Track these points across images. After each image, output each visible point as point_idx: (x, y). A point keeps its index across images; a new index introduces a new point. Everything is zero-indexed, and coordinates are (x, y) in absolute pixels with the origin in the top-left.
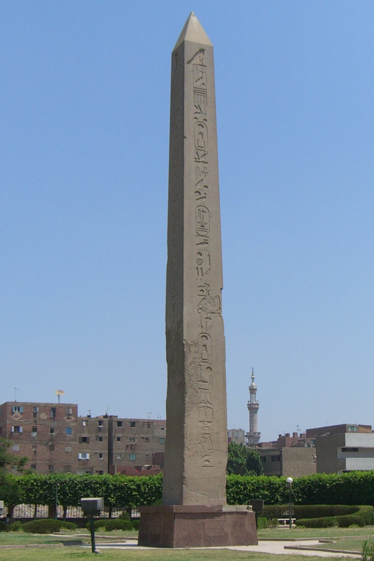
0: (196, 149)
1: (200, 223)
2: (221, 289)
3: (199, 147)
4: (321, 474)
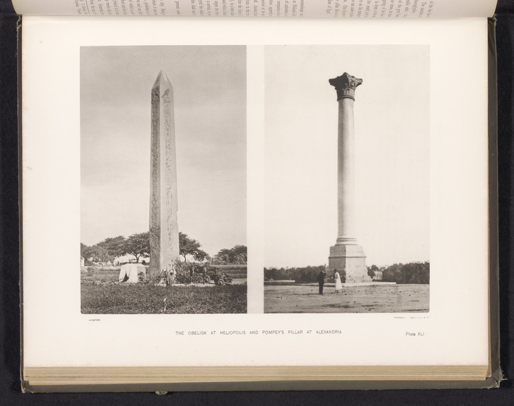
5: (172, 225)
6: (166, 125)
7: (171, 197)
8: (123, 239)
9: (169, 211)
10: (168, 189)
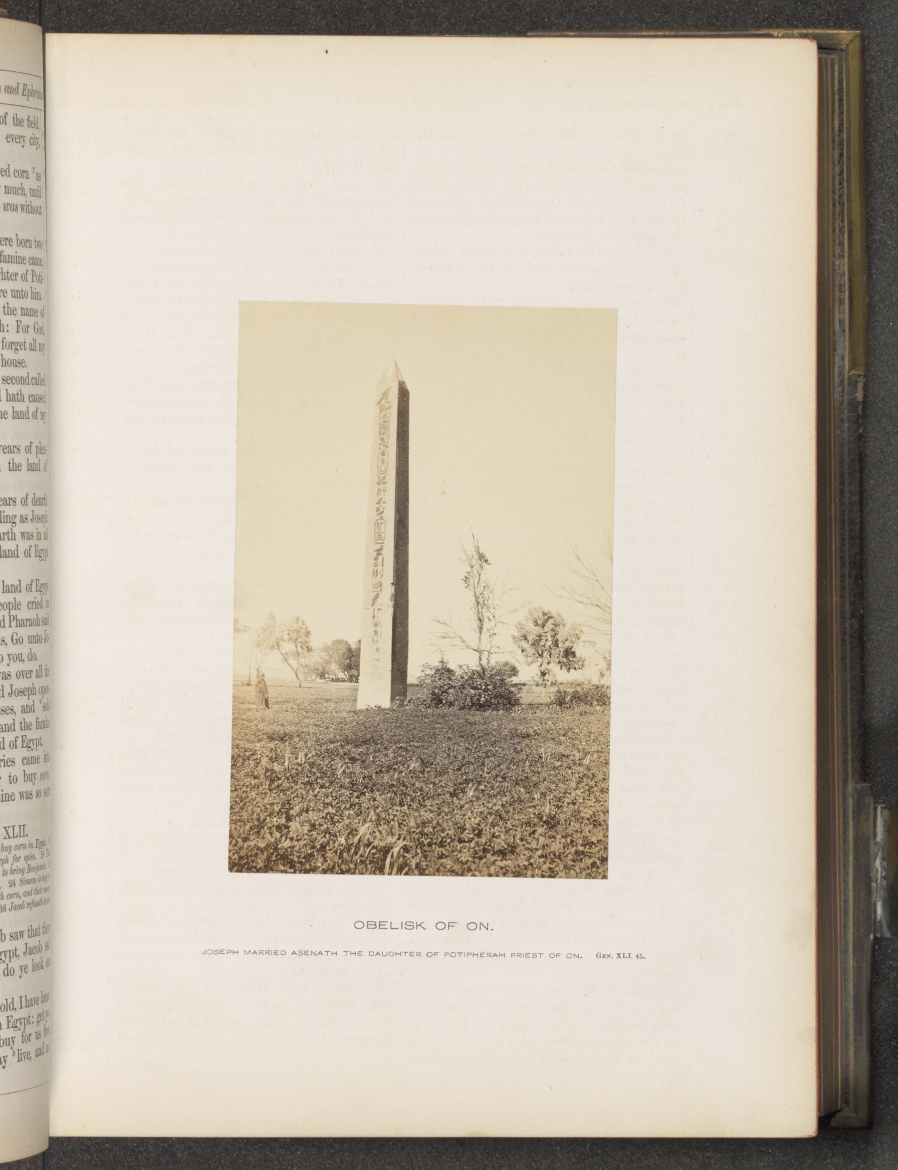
5: (381, 609)
9: (376, 587)
10: (378, 550)
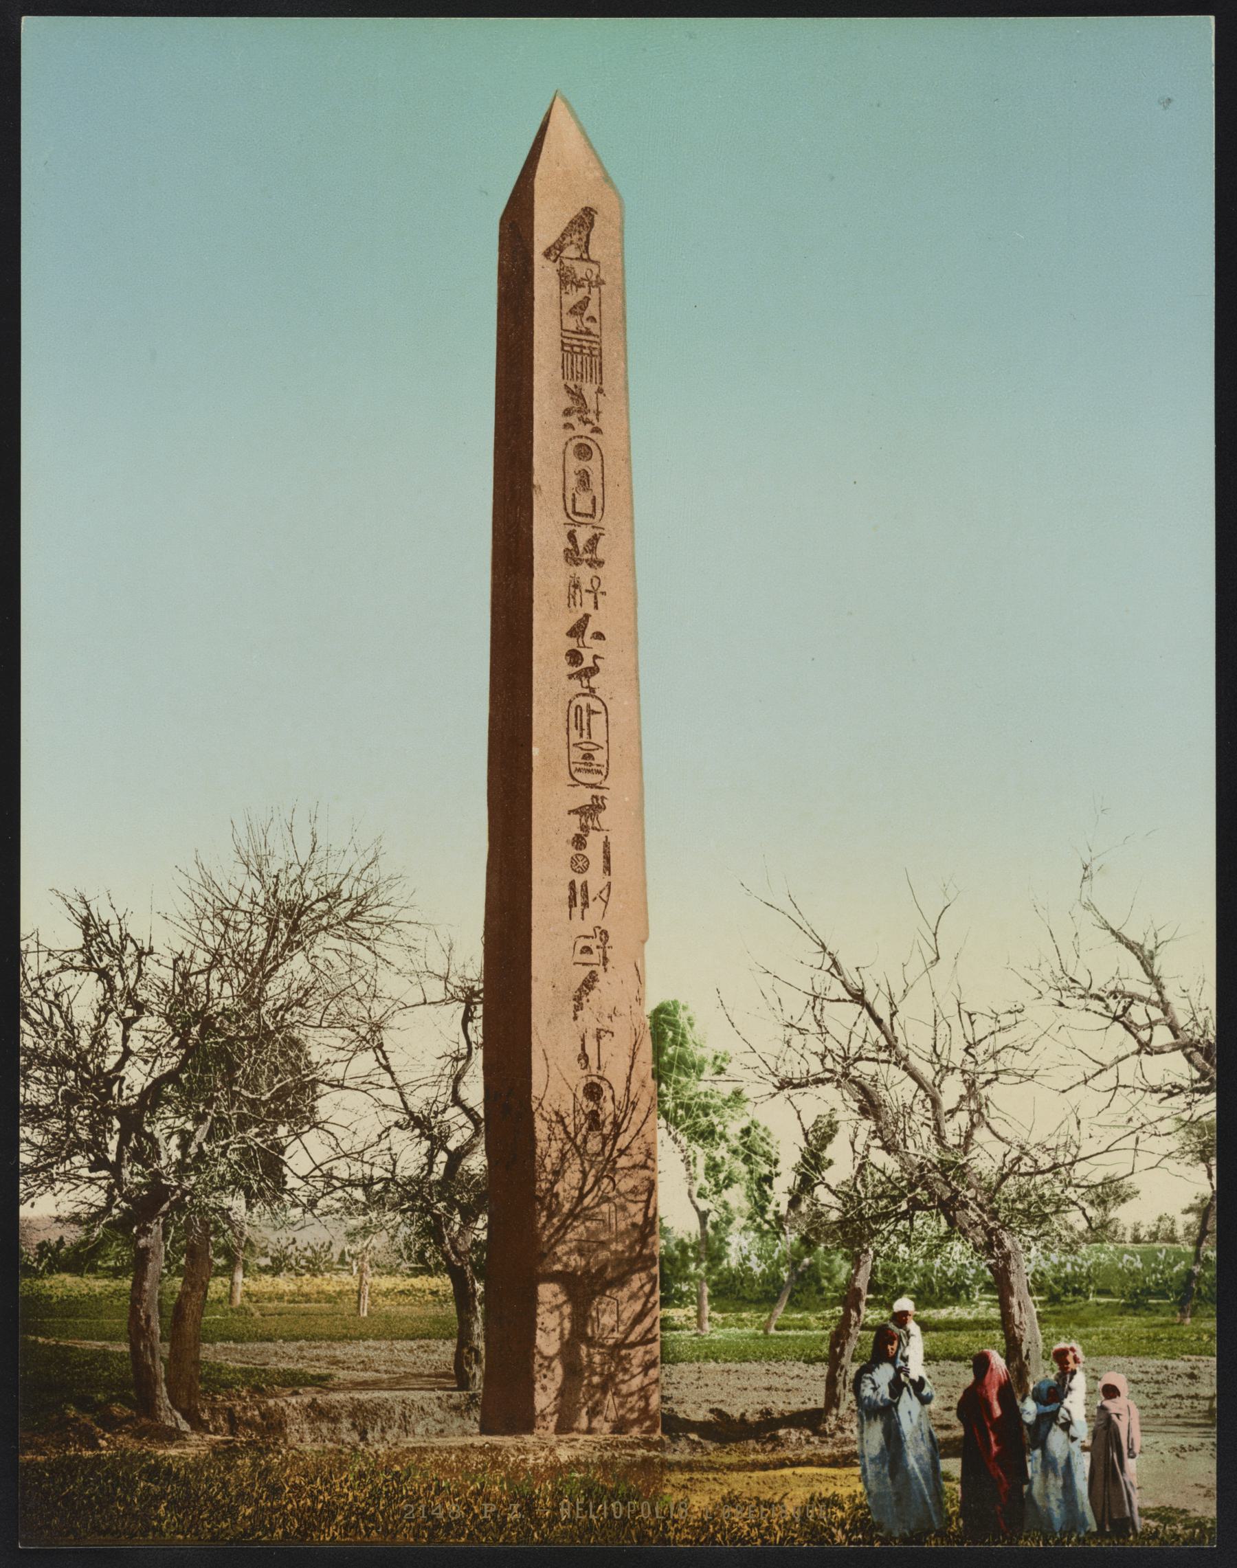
0: (570, 521)
1: (582, 749)
2: (644, 942)
3: (575, 513)
4: (629, 1489)
6: (573, 419)
7: (607, 859)
8: (1206, 1198)
9: (587, 950)
